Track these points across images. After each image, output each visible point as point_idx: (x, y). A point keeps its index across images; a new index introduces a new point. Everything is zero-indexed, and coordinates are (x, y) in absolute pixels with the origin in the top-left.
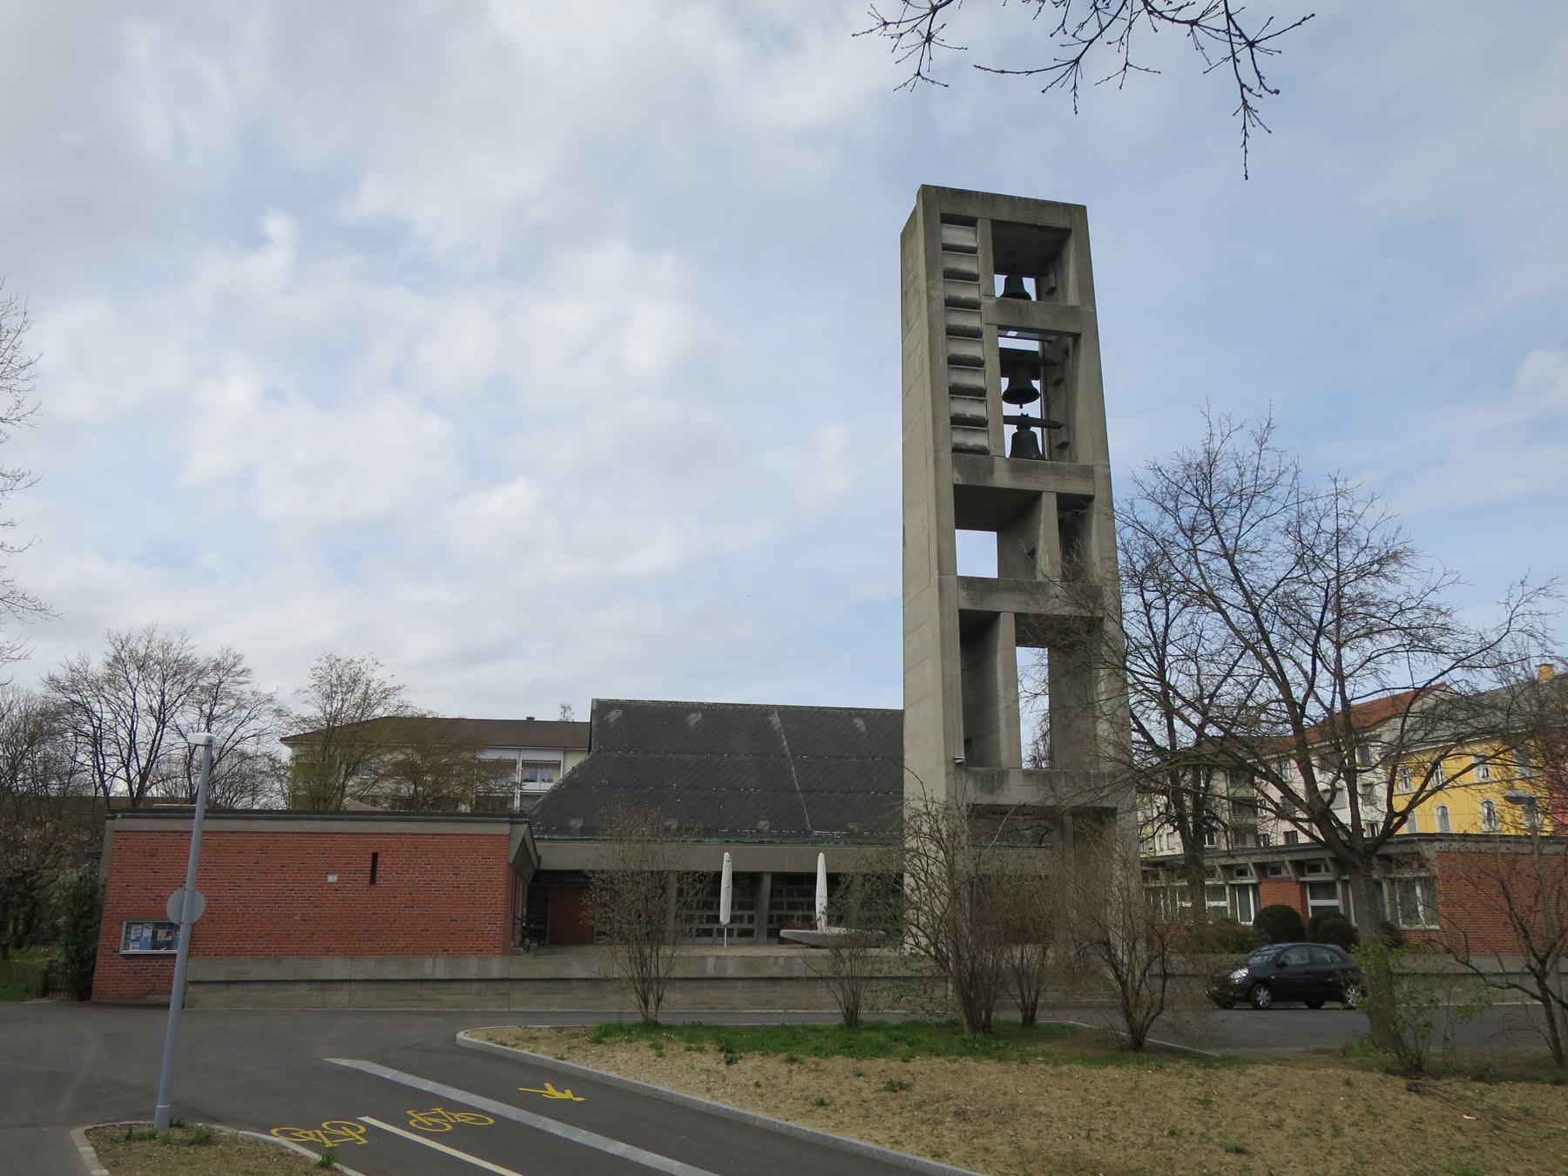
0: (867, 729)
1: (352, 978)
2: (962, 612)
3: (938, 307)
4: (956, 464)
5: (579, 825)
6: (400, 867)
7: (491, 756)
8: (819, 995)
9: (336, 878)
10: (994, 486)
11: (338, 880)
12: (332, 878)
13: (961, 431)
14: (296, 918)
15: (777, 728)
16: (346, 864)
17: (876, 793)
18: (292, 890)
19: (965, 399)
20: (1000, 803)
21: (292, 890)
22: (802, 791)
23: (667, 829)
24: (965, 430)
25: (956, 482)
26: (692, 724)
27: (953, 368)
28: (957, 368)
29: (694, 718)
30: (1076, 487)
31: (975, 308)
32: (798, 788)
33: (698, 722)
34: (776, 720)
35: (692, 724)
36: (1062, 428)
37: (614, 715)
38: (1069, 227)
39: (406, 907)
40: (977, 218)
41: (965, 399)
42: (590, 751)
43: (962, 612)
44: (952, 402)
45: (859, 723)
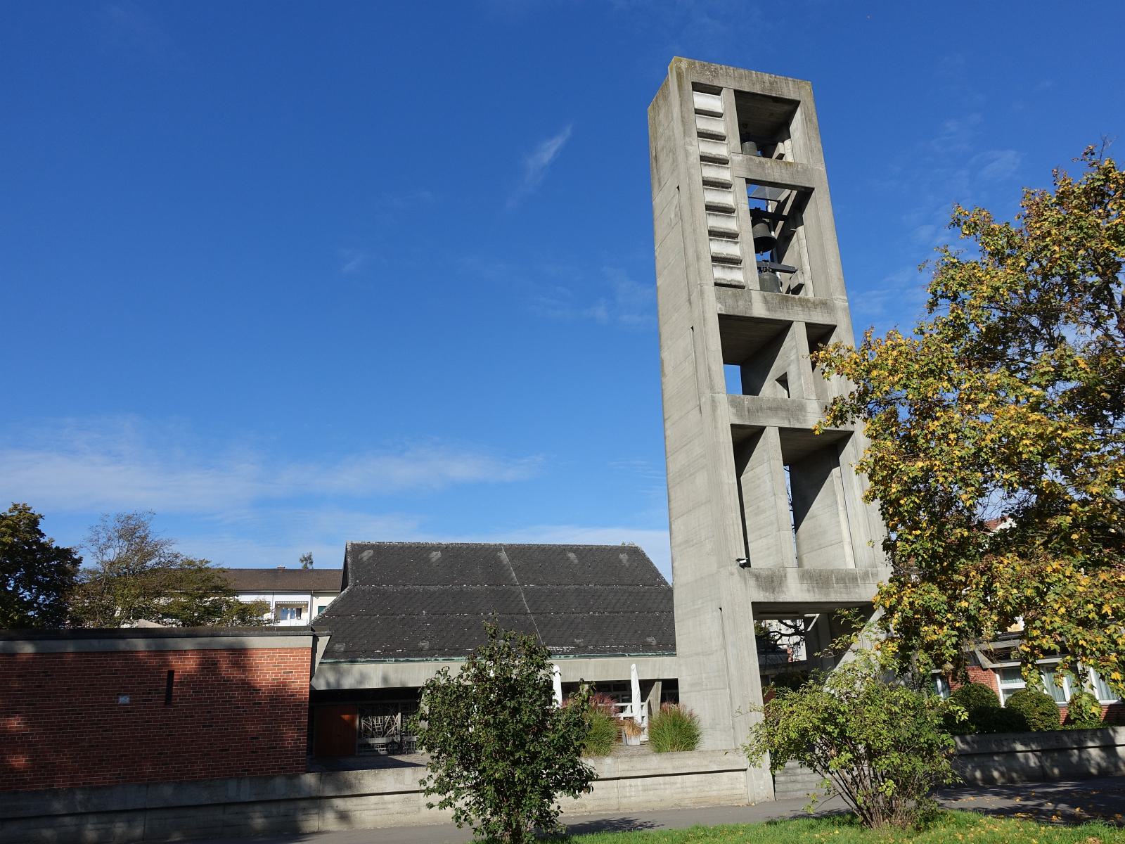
0: (579, 561)
1: (148, 807)
2: (733, 426)
3: (695, 161)
4: (718, 299)
5: (342, 649)
6: (197, 685)
7: (245, 599)
8: (628, 794)
9: (128, 699)
10: (753, 316)
11: (131, 701)
12: (124, 700)
13: (720, 268)
14: (83, 744)
15: (505, 562)
16: (139, 683)
17: (594, 613)
18: (79, 714)
19: (722, 240)
20: (781, 600)
21: (79, 714)
22: (533, 613)
23: (422, 649)
24: (724, 267)
25: (720, 312)
26: (434, 560)
27: (709, 214)
28: (714, 214)
29: (436, 556)
30: (819, 318)
31: (724, 164)
32: (529, 611)
33: (439, 559)
34: (503, 555)
35: (434, 560)
36: (798, 272)
37: (366, 555)
38: (798, 99)
39: (203, 727)
40: (722, 88)
41: (722, 240)
42: (344, 586)
43: (733, 426)
44: (711, 242)
45: (572, 556)
